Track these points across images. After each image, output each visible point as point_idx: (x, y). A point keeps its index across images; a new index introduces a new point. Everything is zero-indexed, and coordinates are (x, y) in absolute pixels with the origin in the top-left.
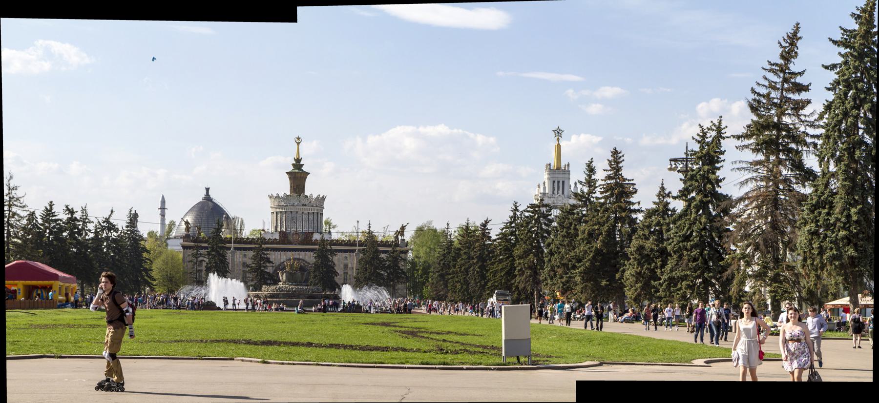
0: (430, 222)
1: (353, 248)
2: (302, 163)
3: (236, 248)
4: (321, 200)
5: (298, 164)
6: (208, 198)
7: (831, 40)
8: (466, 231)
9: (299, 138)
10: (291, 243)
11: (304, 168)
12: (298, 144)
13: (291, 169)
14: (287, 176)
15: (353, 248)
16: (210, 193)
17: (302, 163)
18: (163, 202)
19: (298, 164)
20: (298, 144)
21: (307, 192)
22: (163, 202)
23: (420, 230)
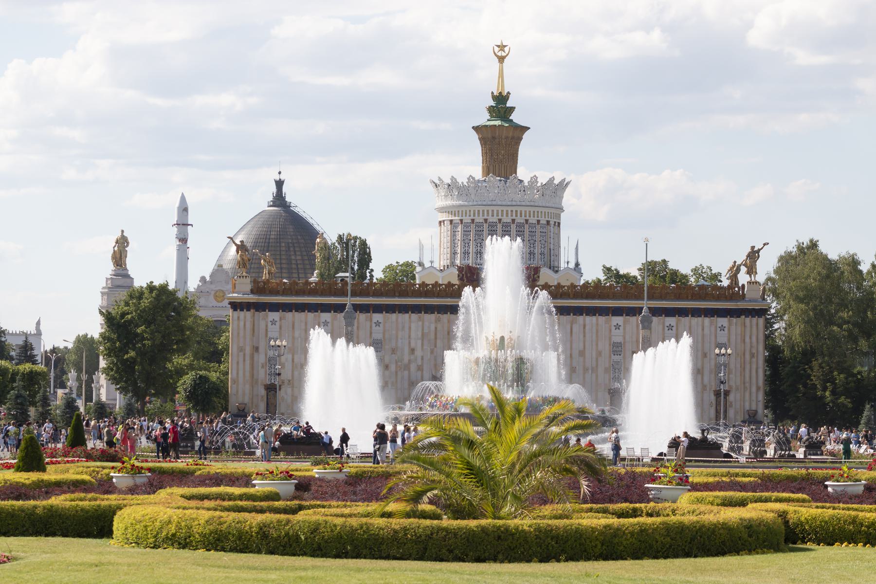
0: (152, 282)
1: (359, 300)
2: (509, 104)
3: (358, 308)
4: (556, 189)
5: (501, 106)
6: (279, 199)
7: (122, 242)
8: (779, 261)
9: (502, 47)
11: (515, 117)
12: (501, 59)
13: (484, 118)
14: (475, 137)
15: (359, 300)
16: (285, 189)
18: (184, 209)
19: (501, 106)
20: (501, 59)
21: (523, 172)
22: (184, 209)
23: (786, 260)
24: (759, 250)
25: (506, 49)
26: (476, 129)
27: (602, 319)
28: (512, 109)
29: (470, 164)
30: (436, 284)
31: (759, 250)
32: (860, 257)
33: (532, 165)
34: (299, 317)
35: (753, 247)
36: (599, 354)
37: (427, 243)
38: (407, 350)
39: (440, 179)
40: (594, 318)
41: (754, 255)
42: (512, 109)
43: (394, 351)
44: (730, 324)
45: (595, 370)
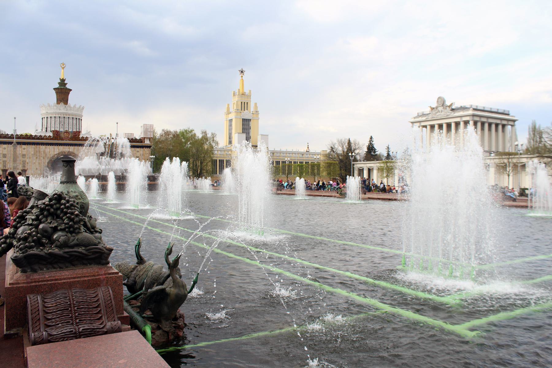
2: (65, 82)
5: (63, 82)
10: (62, 139)
17: (65, 82)
19: (63, 82)
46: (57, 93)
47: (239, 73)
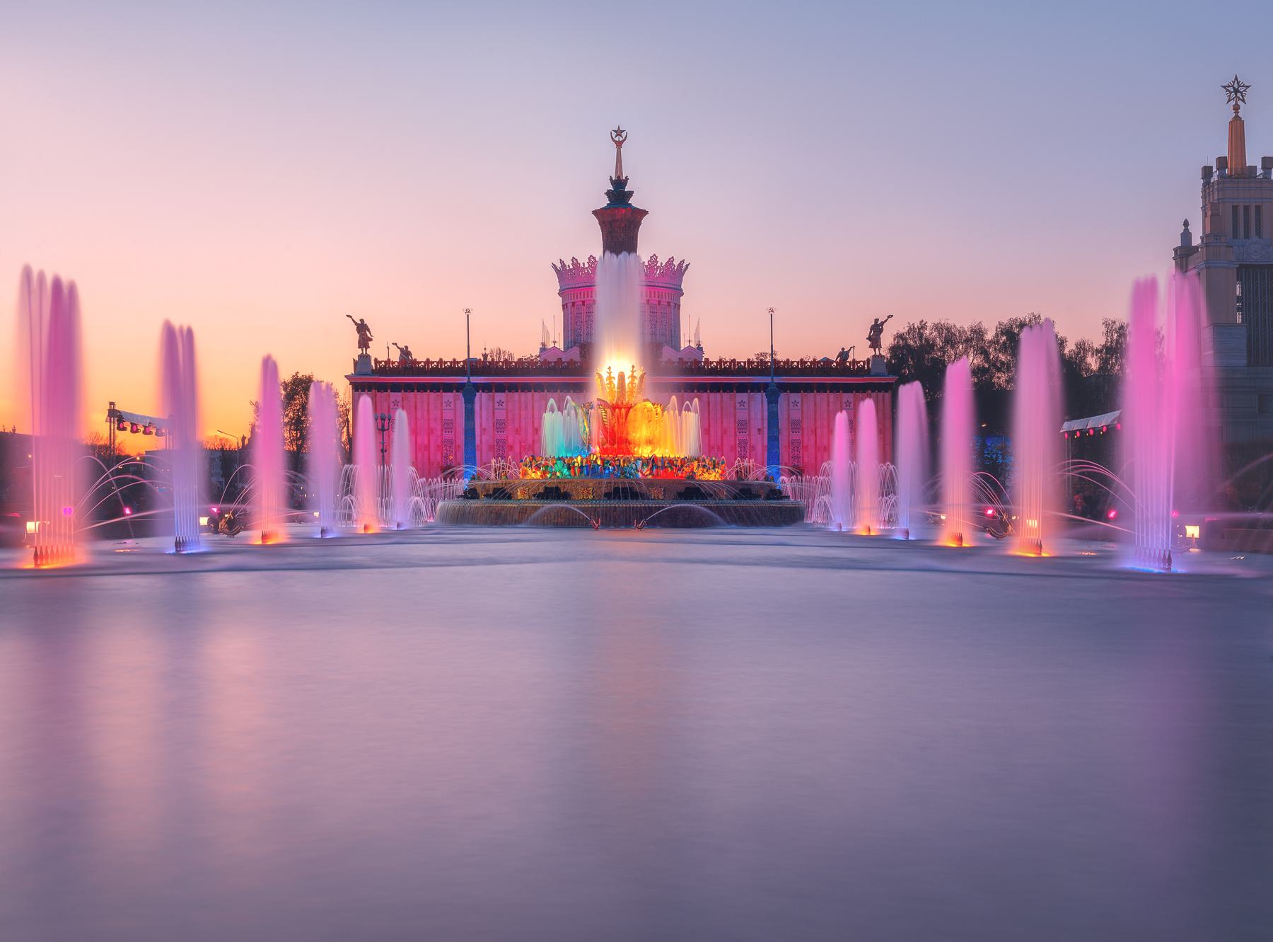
5: (619, 192)
9: (619, 132)
11: (633, 201)
12: (619, 144)
19: (619, 192)
20: (619, 144)
24: (882, 323)
25: (624, 134)
26: (595, 213)
27: (726, 395)
28: (631, 193)
29: (587, 244)
30: (802, 362)
31: (882, 323)
32: (985, 325)
33: (653, 243)
34: (821, 397)
35: (877, 320)
36: (724, 432)
37: (628, 374)
38: (530, 430)
39: (562, 262)
40: (718, 395)
41: (877, 329)
42: (631, 193)
43: (518, 431)
44: (455, 400)
45: (720, 449)
46: (602, 223)
47: (1224, 95)
